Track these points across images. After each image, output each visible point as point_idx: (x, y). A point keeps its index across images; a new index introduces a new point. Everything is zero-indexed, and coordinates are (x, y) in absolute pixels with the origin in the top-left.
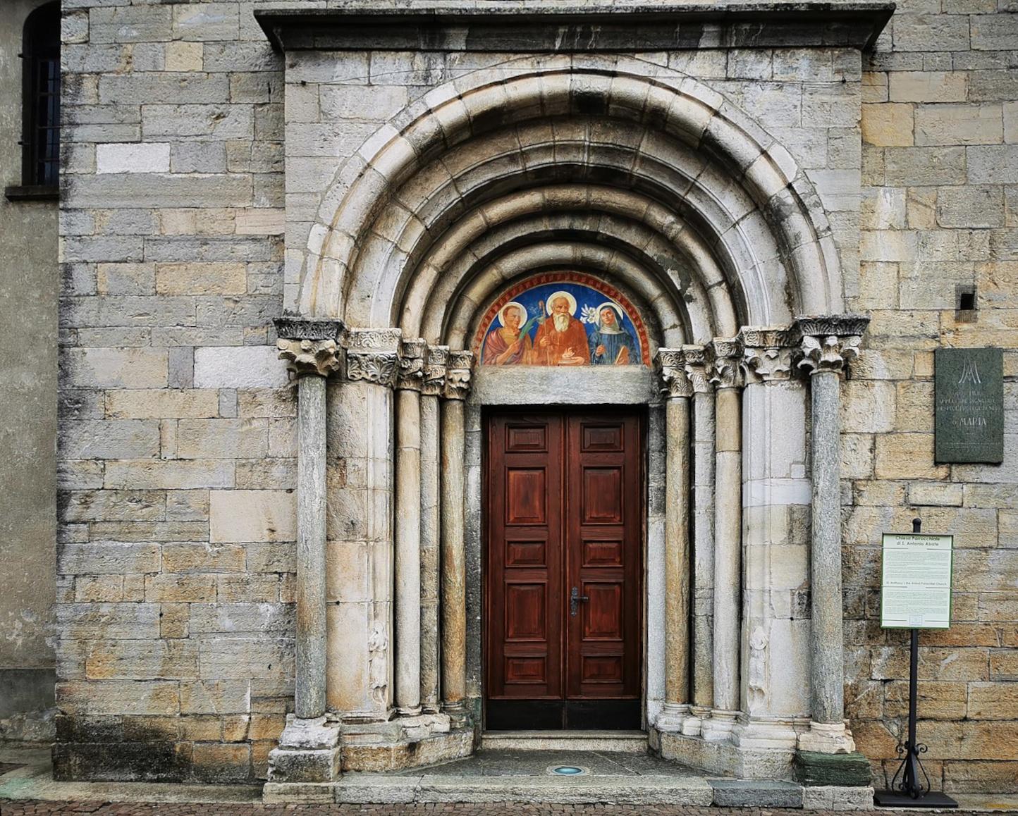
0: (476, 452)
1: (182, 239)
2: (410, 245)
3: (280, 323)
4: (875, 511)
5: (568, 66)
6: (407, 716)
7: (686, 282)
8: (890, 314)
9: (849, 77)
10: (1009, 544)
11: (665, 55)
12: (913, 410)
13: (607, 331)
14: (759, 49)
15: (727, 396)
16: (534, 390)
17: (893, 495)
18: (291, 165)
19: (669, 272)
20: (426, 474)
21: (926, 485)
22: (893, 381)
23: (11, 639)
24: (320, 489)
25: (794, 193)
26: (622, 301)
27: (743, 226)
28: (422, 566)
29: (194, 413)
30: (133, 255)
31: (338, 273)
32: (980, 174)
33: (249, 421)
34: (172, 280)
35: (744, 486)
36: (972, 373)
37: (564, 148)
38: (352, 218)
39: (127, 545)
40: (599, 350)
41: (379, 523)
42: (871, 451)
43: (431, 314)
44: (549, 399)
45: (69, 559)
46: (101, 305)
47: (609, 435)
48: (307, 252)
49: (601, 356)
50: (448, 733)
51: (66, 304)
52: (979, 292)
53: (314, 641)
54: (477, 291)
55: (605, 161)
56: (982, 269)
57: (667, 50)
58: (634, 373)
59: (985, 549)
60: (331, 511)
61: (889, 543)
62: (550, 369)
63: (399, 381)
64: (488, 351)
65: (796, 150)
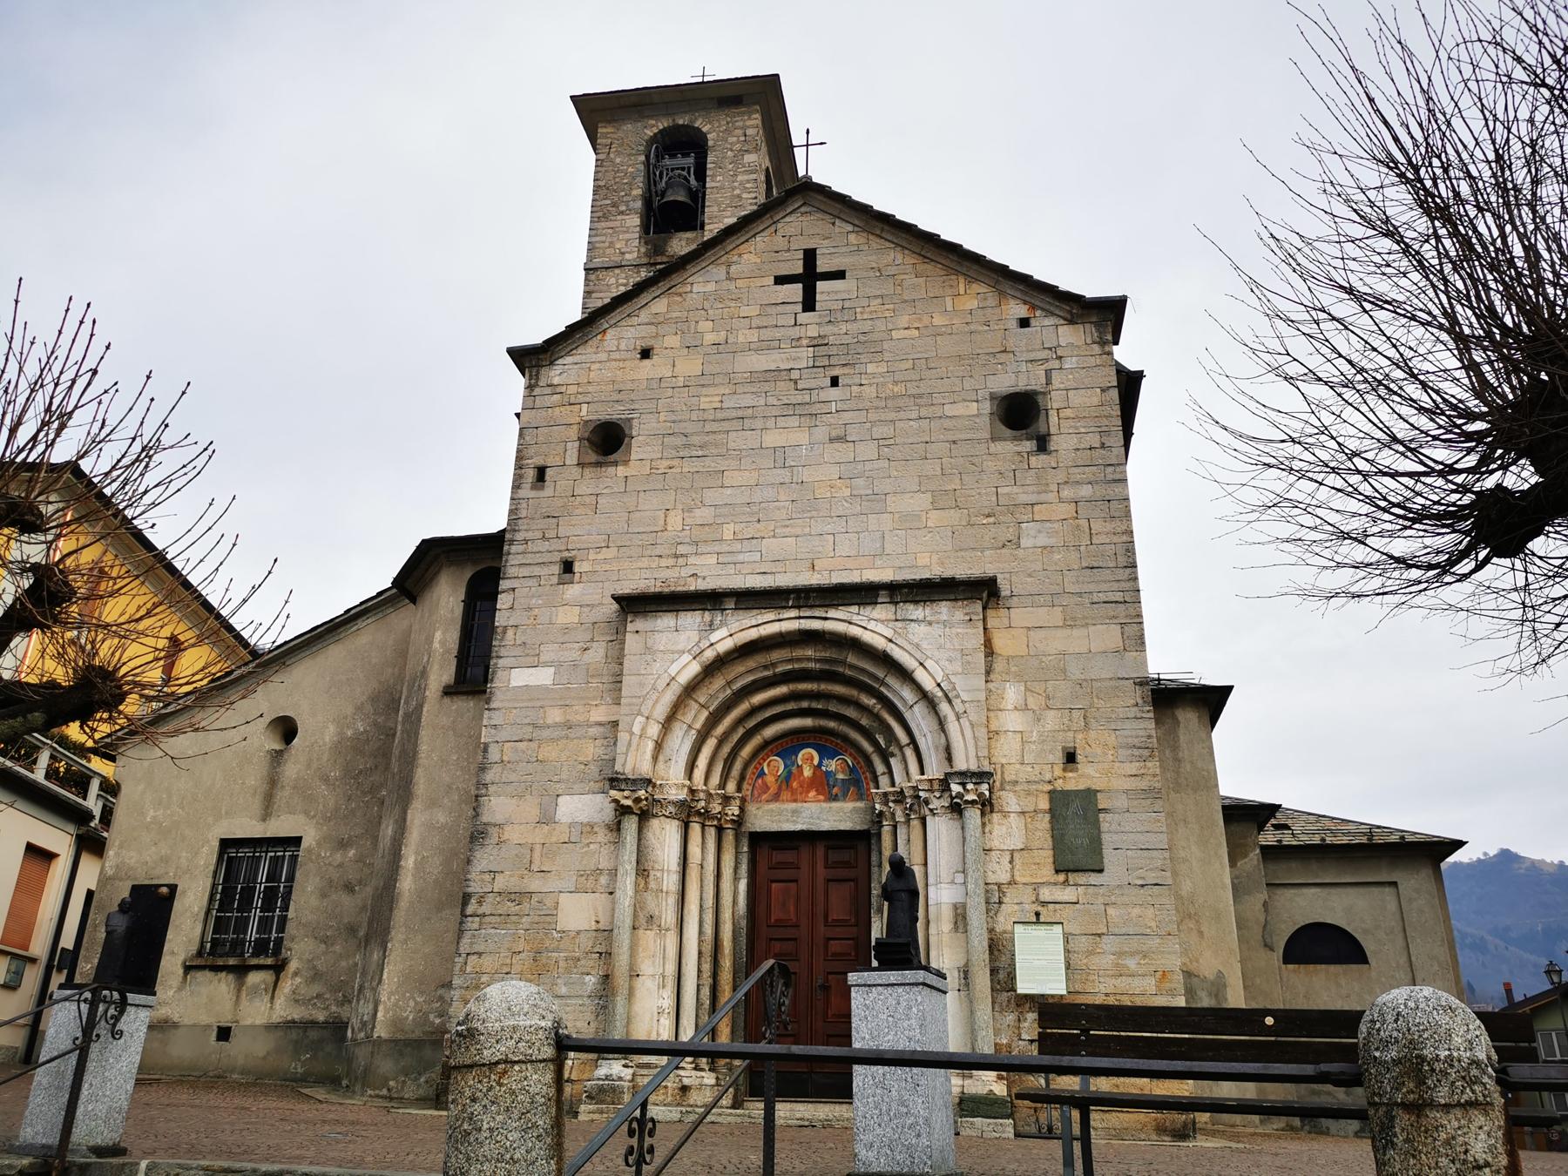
0: (744, 868)
1: (556, 725)
2: (698, 725)
3: (612, 780)
4: (1016, 907)
5: (797, 615)
6: (683, 1068)
7: (889, 743)
8: (1018, 766)
9: (974, 617)
10: (1116, 931)
11: (857, 607)
12: (1039, 834)
13: (840, 776)
14: (916, 602)
15: (915, 823)
16: (788, 820)
17: (1027, 896)
18: (626, 679)
19: (877, 736)
20: (706, 882)
21: (1051, 887)
22: (1023, 813)
23: (405, 1015)
24: (630, 892)
25: (942, 689)
26: (851, 755)
27: (916, 708)
28: (700, 953)
29: (554, 839)
30: (527, 737)
31: (650, 745)
32: (1075, 672)
33: (588, 845)
34: (549, 752)
35: (1405, 944)
36: (1076, 805)
37: (799, 660)
38: (661, 711)
39: (503, 932)
40: (835, 790)
41: (669, 917)
42: (1011, 862)
43: (714, 769)
44: (799, 827)
45: (465, 941)
46: (503, 769)
47: (845, 855)
48: (632, 734)
49: (836, 795)
50: (713, 1086)
51: (483, 769)
52: (1078, 752)
53: (620, 1001)
54: (746, 751)
55: (827, 667)
56: (1080, 736)
57: (859, 604)
58: (860, 808)
59: (1099, 935)
60: (637, 907)
61: (1019, 929)
62: (800, 805)
63: (689, 815)
64: (756, 792)
65: (941, 663)
